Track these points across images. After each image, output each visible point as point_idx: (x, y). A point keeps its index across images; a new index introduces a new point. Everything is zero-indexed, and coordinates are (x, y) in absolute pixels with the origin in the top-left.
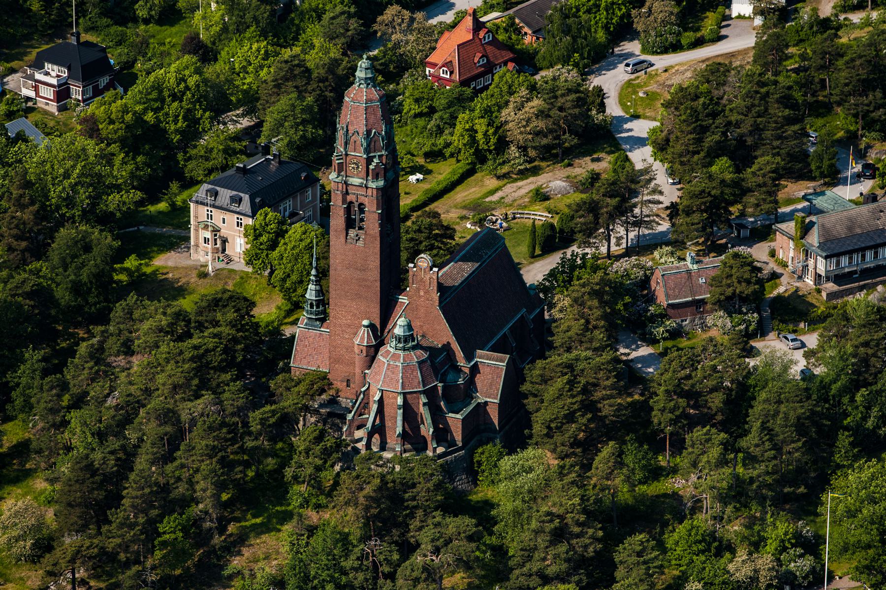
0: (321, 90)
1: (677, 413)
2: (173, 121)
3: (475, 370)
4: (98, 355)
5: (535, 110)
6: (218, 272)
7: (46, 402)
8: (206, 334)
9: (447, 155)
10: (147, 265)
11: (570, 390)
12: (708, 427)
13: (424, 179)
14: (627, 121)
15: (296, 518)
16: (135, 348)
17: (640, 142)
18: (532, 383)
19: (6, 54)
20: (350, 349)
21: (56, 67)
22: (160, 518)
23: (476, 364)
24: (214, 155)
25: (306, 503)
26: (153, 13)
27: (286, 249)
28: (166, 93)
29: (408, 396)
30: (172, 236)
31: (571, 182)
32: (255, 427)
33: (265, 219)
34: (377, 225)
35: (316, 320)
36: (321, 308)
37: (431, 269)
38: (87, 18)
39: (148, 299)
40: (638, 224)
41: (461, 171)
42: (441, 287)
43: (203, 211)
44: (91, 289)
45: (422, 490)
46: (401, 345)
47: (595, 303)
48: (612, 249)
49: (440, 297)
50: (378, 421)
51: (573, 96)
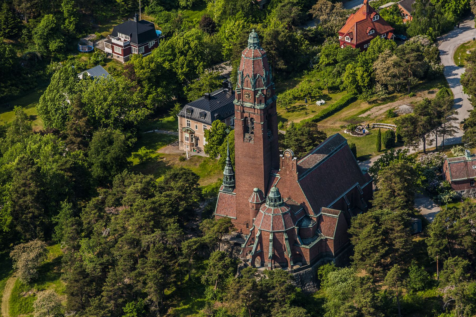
0: (268, 49)
1: (441, 248)
2: (180, 67)
3: (320, 219)
4: (100, 207)
5: (392, 62)
6: (192, 158)
7: (69, 233)
8: (162, 195)
9: (341, 89)
10: (152, 152)
11: (375, 232)
12: (457, 257)
13: (326, 103)
14: (454, 68)
15: (207, 305)
16: (122, 202)
17: (457, 82)
18: (354, 227)
19: (100, 27)
20: (247, 205)
21: (124, 35)
22: (124, 304)
23: (321, 216)
24: (204, 88)
25: (215, 297)
26: (189, 3)
27: (227, 145)
28: (177, 51)
29: (276, 234)
30: (171, 136)
31: (413, 106)
32: (185, 251)
33: (216, 126)
34: (261, 131)
35: (230, 187)
36: (232, 180)
37: (293, 158)
38: (150, 6)
39: (134, 174)
40: (444, 132)
41: (347, 99)
42: (300, 169)
43: (185, 121)
44: (112, 167)
45: (278, 291)
46: (272, 204)
47: (398, 179)
48: (426, 148)
49: (298, 175)
50: (259, 249)
51: (415, 54)
